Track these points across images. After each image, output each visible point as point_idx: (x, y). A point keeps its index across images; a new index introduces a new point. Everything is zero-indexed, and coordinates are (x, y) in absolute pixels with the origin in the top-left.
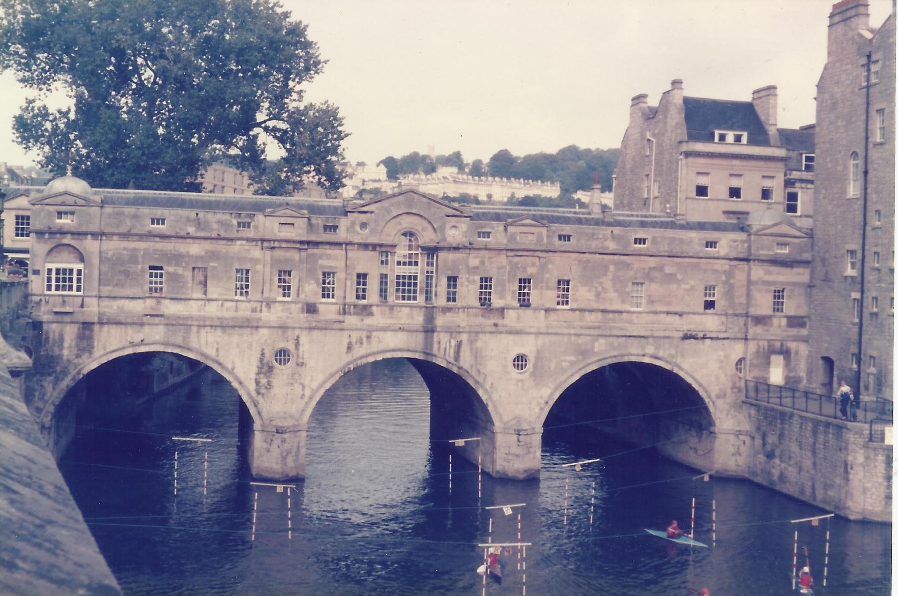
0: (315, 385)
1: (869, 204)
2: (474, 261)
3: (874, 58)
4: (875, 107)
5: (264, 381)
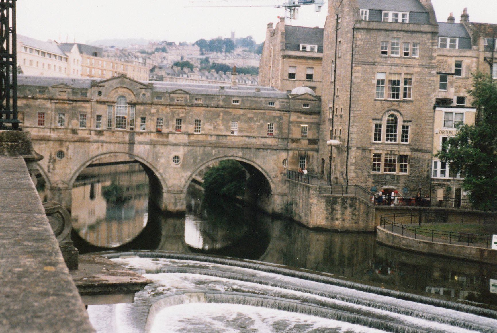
1: (336, 85)
2: (153, 110)
3: (339, 17)
4: (339, 40)
5: (51, 166)
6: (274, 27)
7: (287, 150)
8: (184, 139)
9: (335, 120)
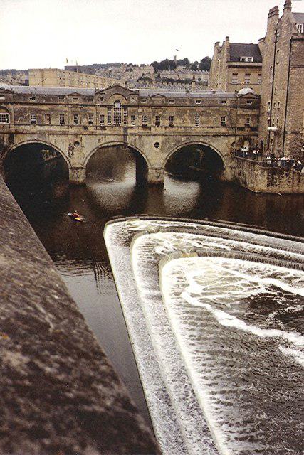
0: (87, 154)
2: (140, 111)
5: (71, 152)
6: (221, 45)
7: (235, 135)
8: (163, 131)
9: (273, 112)
